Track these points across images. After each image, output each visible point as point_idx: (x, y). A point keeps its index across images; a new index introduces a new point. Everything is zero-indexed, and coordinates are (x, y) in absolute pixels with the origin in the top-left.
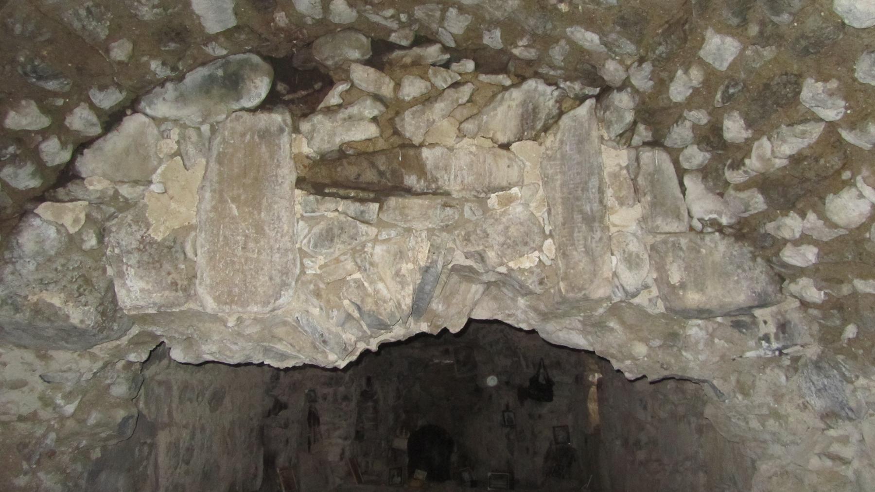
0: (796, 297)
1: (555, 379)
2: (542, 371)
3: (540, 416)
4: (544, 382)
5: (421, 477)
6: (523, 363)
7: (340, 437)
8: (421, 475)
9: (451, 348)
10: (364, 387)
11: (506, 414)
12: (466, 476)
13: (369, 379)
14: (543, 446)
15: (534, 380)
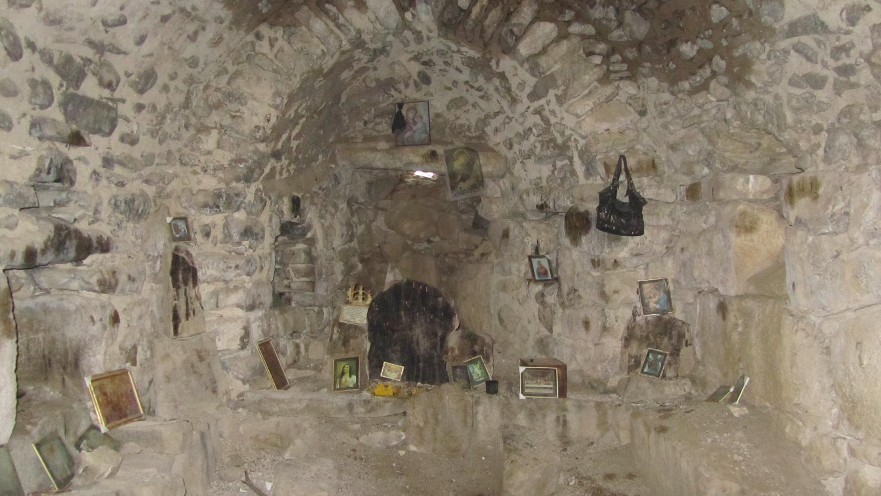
0: (107, 377)
1: (647, 194)
2: (622, 177)
3: (616, 263)
4: (626, 200)
5: (393, 376)
6: (579, 168)
7: (239, 306)
8: (393, 371)
9: (440, 150)
10: (287, 216)
11: (535, 261)
12: (476, 371)
13: (296, 204)
14: (620, 316)
15: (607, 198)
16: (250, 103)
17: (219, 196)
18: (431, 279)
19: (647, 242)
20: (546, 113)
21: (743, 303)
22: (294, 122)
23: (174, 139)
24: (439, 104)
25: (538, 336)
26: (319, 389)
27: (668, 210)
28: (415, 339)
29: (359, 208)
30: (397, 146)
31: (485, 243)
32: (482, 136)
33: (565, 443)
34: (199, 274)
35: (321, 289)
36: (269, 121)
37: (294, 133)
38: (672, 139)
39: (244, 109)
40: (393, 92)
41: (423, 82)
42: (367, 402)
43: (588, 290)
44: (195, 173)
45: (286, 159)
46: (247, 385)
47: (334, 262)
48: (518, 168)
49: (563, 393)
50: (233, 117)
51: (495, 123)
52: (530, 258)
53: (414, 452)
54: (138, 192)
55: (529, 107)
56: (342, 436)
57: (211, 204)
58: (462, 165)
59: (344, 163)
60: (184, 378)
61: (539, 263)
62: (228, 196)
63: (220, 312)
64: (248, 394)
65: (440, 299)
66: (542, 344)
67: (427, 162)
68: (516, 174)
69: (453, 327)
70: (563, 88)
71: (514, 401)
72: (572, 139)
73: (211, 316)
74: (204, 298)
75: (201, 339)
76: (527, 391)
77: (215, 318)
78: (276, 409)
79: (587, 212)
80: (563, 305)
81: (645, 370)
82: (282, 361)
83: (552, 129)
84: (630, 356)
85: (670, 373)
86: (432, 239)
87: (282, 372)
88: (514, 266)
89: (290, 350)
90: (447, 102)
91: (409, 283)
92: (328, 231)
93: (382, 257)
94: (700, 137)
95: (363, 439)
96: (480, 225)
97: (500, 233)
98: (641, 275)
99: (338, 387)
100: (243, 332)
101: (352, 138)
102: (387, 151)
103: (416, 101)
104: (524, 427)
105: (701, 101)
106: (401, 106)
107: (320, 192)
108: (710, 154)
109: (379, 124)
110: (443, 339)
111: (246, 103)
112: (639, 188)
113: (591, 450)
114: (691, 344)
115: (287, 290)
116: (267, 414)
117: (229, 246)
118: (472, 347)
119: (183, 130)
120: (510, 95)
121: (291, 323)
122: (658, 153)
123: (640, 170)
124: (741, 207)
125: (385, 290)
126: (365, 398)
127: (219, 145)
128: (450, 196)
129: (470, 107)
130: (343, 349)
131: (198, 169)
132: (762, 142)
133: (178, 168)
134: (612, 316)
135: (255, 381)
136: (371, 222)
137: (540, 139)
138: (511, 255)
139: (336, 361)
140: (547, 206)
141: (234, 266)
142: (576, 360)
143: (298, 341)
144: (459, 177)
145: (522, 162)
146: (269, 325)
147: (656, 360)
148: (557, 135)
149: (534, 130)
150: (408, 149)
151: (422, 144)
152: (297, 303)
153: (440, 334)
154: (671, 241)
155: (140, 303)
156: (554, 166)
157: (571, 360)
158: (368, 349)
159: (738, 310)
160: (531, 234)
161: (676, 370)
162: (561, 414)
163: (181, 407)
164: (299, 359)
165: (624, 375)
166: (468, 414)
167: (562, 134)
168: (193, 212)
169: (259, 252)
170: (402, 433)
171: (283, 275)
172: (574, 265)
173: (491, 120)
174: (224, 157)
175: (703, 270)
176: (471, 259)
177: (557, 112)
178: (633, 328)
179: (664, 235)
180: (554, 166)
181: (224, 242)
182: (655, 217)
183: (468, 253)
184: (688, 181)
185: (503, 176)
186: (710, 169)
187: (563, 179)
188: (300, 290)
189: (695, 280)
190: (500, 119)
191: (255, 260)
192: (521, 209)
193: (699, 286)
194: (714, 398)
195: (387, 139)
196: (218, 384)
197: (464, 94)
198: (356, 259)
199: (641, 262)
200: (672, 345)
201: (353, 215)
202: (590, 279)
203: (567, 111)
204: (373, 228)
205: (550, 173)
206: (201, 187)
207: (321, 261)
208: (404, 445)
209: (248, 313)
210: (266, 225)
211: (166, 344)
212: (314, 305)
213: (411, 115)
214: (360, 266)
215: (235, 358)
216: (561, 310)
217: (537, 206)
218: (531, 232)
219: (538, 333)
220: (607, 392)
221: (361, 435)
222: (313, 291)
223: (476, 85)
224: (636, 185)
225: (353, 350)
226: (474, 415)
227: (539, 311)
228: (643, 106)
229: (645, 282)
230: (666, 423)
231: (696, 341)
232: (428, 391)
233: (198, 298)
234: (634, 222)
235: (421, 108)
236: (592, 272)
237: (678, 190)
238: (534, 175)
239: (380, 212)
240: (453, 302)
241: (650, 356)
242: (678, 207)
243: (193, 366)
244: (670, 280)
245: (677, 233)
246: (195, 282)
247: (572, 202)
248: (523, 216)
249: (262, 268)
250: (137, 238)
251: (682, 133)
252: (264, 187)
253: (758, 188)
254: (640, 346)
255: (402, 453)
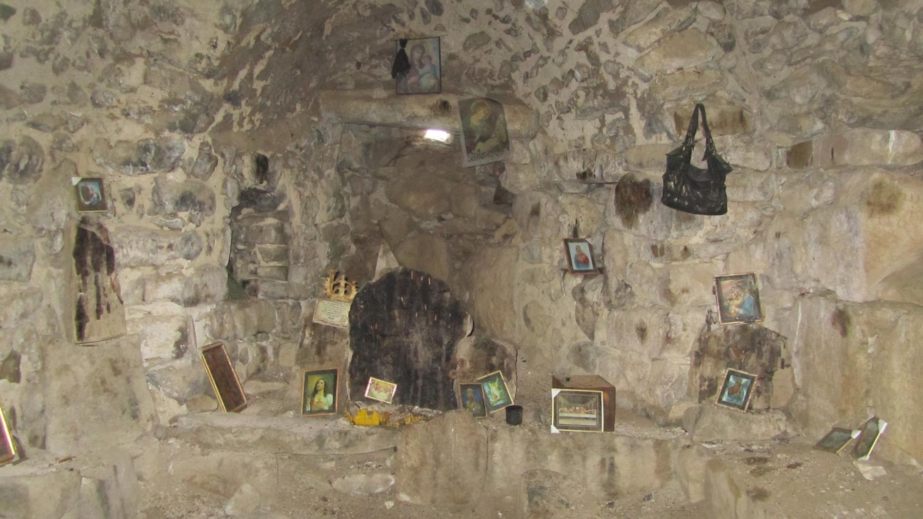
1: (732, 158)
2: (699, 135)
3: (686, 252)
4: (703, 165)
5: (382, 396)
6: (638, 123)
7: (174, 300)
8: (382, 390)
9: (453, 101)
10: (250, 181)
11: (573, 246)
12: (493, 391)
13: (262, 166)
14: (690, 323)
15: (678, 162)
16: (188, 21)
17: (146, 149)
18: (440, 268)
19: (729, 224)
20: (595, 48)
21: (879, 314)
22: (257, 52)
23: (80, 69)
24: (454, 41)
25: (574, 343)
26: (285, 410)
27: (758, 181)
28: (412, 347)
29: (353, 175)
30: (398, 95)
31: (509, 222)
32: (508, 85)
33: (610, 494)
34: (118, 256)
35: (298, 277)
36: (215, 47)
37: (257, 70)
38: (768, 83)
39: (180, 30)
40: (394, 25)
41: (433, 12)
42: (343, 434)
43: (645, 287)
44: (113, 117)
45: (247, 104)
46: (184, 406)
47: (316, 242)
48: (553, 126)
49: (610, 426)
50: (166, 41)
51: (526, 66)
52: (566, 241)
53: (407, 504)
54: (18, 140)
55: (571, 42)
56: (310, 479)
57: (135, 160)
58: (481, 121)
59: (330, 115)
60: (91, 398)
61: (578, 248)
62: (159, 149)
63: (147, 308)
64: (184, 419)
65: (447, 295)
66: (580, 355)
67: (436, 115)
68: (551, 134)
69: (462, 334)
70: (620, 9)
71: (543, 437)
72: (630, 83)
73: (133, 312)
74: (124, 287)
75: (118, 346)
76: (561, 422)
77: (141, 315)
78: (220, 441)
79: (647, 182)
80: (609, 304)
81: (724, 399)
82: (240, 371)
83: (602, 70)
84: (703, 379)
85: (758, 404)
86: (443, 216)
87: (237, 387)
88: (546, 252)
89: (252, 354)
90: (463, 39)
91: (406, 273)
92: (308, 205)
93: (379, 235)
94: (814, 77)
95: (337, 483)
96: (503, 199)
97: (529, 209)
98: (719, 268)
99: (308, 409)
100: (179, 334)
101: (341, 84)
102: (385, 101)
103: (423, 37)
104: (557, 474)
105: (824, 22)
106: (403, 43)
107: (297, 151)
108: (829, 101)
109: (376, 67)
110: (451, 347)
111: (183, 22)
112: (722, 149)
113: (647, 508)
114: (788, 366)
115: (253, 277)
116: (207, 447)
117: (160, 218)
118: (489, 359)
119: (95, 57)
120: (546, 25)
121: (255, 321)
122: (747, 102)
123: (723, 125)
124: (876, 176)
125: (374, 281)
126: (341, 427)
127: (146, 81)
128: (466, 162)
129: (493, 46)
130: (317, 358)
131: (117, 112)
132: (913, 81)
133: (90, 111)
134: (679, 323)
135: (194, 400)
136: (369, 193)
137: (585, 84)
138: (542, 238)
139: (308, 374)
140: (591, 174)
141: (166, 245)
142: (624, 376)
143: (264, 343)
144: (478, 137)
145: (559, 118)
146: (221, 325)
147: (739, 384)
148: (609, 78)
149: (577, 74)
150: (412, 99)
151: (430, 92)
152: (266, 294)
153: (446, 342)
154: (760, 223)
155: (23, 296)
156: (603, 121)
157: (618, 376)
158: (350, 360)
159: (868, 323)
160: (572, 211)
161: (767, 399)
162: (607, 456)
163: (84, 439)
164: (264, 366)
165: (693, 404)
166: (481, 452)
167: (616, 76)
168: (110, 170)
169: (205, 226)
170: (391, 477)
171: (248, 258)
172: (626, 251)
173: (521, 64)
174: (153, 96)
175: (811, 264)
176: (491, 241)
177: (610, 45)
178: (707, 341)
179: (752, 215)
180: (603, 121)
181: (153, 212)
182: (741, 190)
183: (488, 234)
184: (788, 141)
185: (534, 137)
186: (826, 123)
187: (614, 139)
188: (271, 278)
189: (796, 276)
190: (532, 60)
191: (199, 238)
192: (557, 179)
193: (801, 285)
194: (827, 445)
195: (386, 85)
196: (141, 406)
197: (485, 28)
198: (349, 238)
199: (720, 251)
200: (763, 365)
201: (344, 184)
202: (648, 272)
203: (625, 43)
204: (372, 201)
205: (597, 131)
206: (122, 137)
207: (298, 244)
208: (393, 493)
209: (188, 309)
210: (217, 191)
211: (66, 351)
212: (288, 297)
213: (417, 55)
214: (353, 248)
215: (168, 369)
216: (606, 311)
217: (578, 175)
218: (569, 208)
219: (575, 338)
220: (667, 425)
221: (336, 478)
222: (286, 279)
223: (502, 15)
224: (717, 146)
225: (330, 360)
226: (489, 454)
227: (577, 311)
228: (730, 36)
229: (725, 278)
230: (763, 483)
231: (796, 362)
232: (427, 419)
233: (115, 288)
234: (714, 195)
235: (430, 47)
236: (651, 263)
237: (774, 154)
238: (574, 134)
239: (379, 182)
240: (468, 295)
241: (731, 379)
242: (773, 176)
243: (103, 382)
244: (758, 276)
245: (768, 212)
246: (111, 268)
247: (626, 169)
248: (560, 190)
249: (210, 249)
250: (19, 204)
251: (786, 72)
252: (214, 141)
253: (901, 150)
254: (716, 365)
255: (390, 504)
